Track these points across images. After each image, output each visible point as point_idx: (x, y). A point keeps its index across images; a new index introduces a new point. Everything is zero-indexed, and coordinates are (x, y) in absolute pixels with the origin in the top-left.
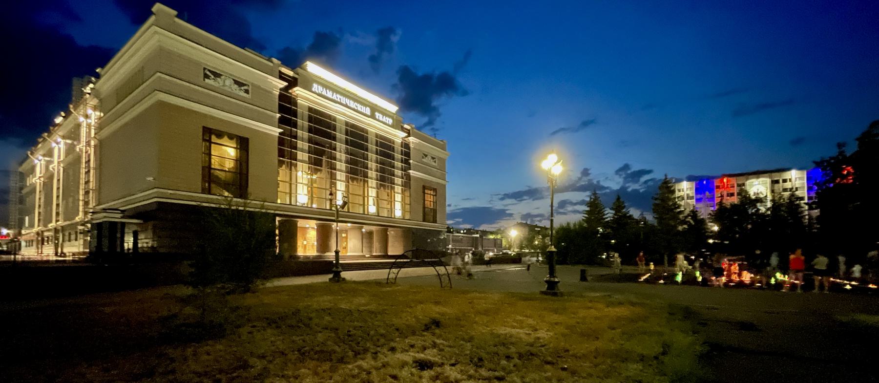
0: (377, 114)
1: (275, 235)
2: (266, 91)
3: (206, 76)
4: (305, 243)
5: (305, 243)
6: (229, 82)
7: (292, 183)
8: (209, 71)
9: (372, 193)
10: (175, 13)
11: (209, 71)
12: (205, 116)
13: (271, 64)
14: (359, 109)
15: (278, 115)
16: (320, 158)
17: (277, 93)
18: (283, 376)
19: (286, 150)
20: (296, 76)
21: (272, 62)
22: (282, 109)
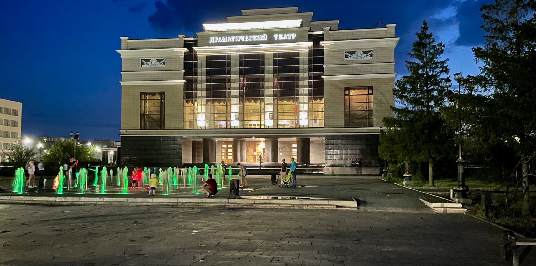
0: (276, 36)
1: (455, 165)
2: (175, 58)
3: (142, 64)
4: (255, 154)
5: (255, 154)
6: (154, 62)
7: (194, 113)
8: (348, 52)
9: (235, 109)
10: (127, 38)
11: (348, 52)
12: (138, 86)
13: (178, 39)
14: (255, 39)
15: (183, 71)
16: (218, 93)
17: (182, 56)
18: (311, 237)
19: (189, 93)
20: (196, 39)
21: (178, 38)
22: (186, 66)
